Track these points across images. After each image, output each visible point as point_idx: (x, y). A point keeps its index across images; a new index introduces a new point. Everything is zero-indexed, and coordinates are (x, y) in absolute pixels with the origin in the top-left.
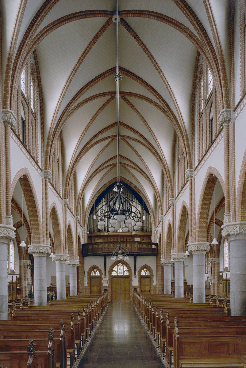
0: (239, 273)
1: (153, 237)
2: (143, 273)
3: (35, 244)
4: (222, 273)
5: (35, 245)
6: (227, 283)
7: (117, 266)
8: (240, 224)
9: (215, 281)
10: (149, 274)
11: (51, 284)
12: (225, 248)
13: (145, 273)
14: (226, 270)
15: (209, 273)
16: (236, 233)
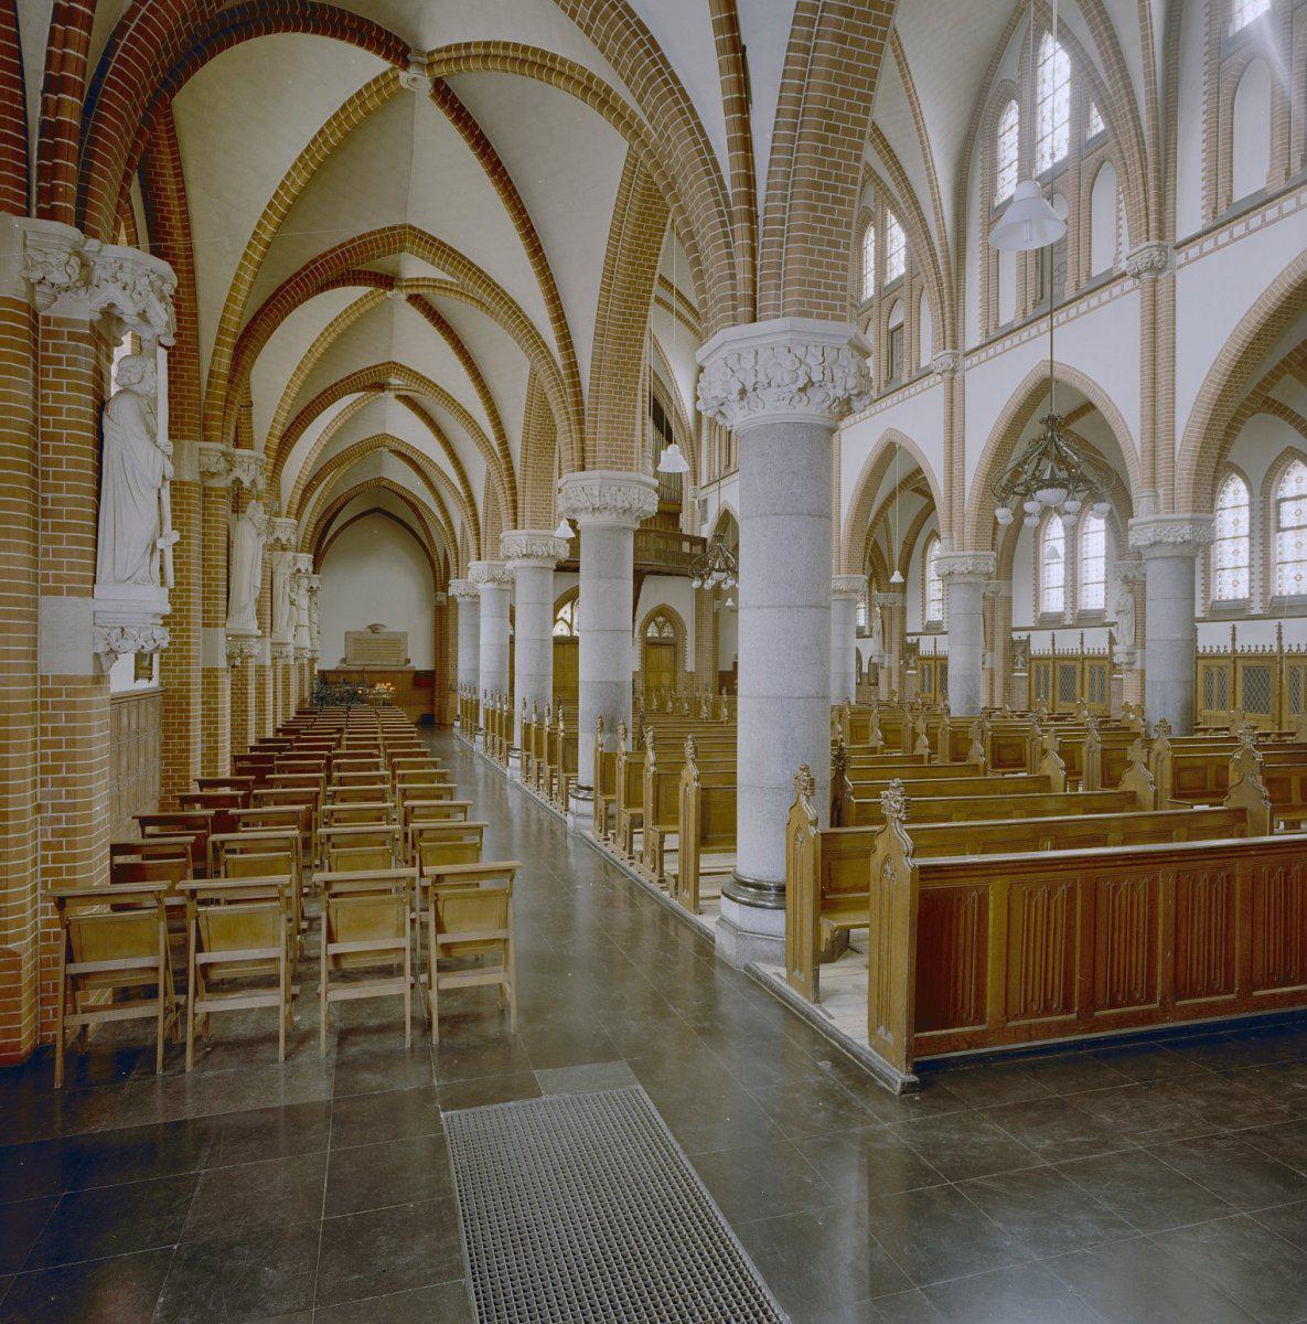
0: (1179, 636)
1: (684, 519)
2: (652, 632)
3: (535, 528)
4: (915, 638)
5: (533, 531)
6: (940, 664)
7: (572, 605)
8: (1192, 521)
9: (892, 661)
10: (672, 635)
11: (344, 661)
12: (927, 567)
13: (660, 630)
14: (933, 629)
15: (874, 634)
16: (1179, 540)
